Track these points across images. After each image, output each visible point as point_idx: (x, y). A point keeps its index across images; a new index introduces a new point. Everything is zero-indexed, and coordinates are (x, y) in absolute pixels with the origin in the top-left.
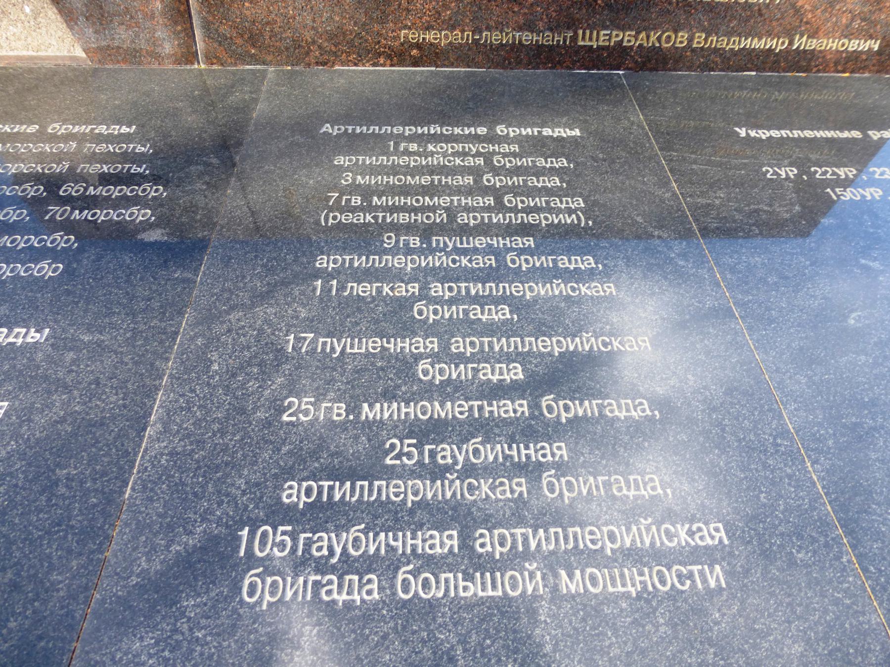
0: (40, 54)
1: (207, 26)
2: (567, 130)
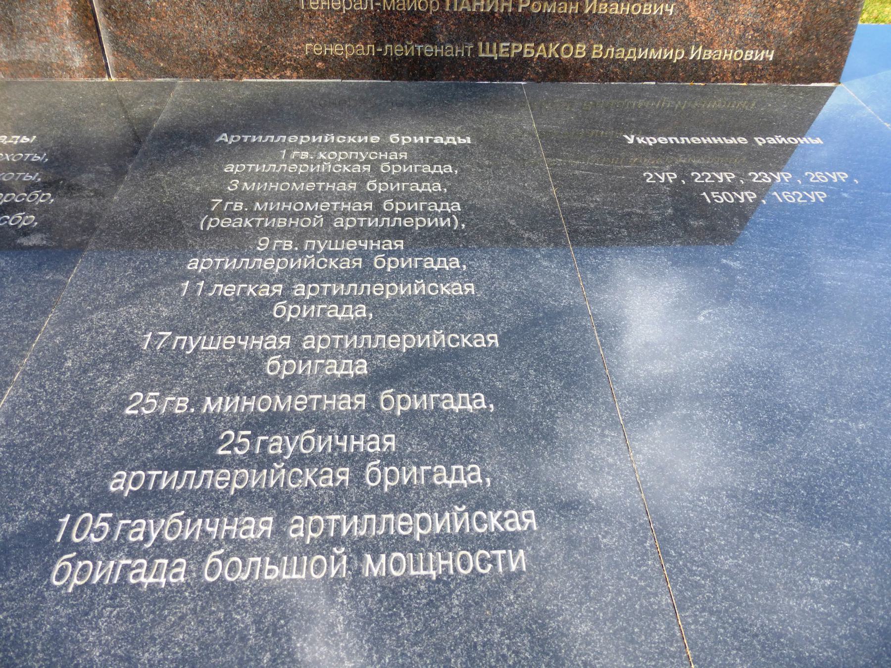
2: (459, 138)
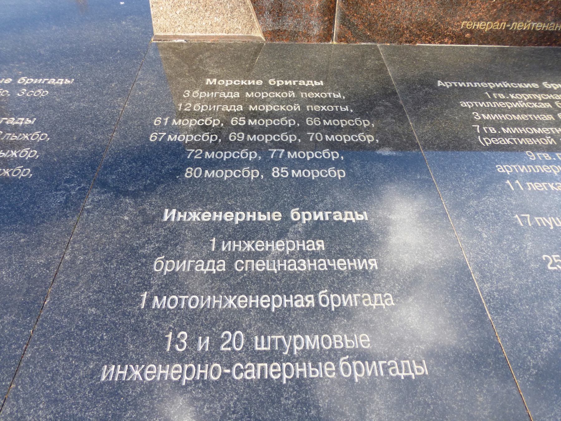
0: (229, 34)
1: (344, 19)
2: (315, 82)
